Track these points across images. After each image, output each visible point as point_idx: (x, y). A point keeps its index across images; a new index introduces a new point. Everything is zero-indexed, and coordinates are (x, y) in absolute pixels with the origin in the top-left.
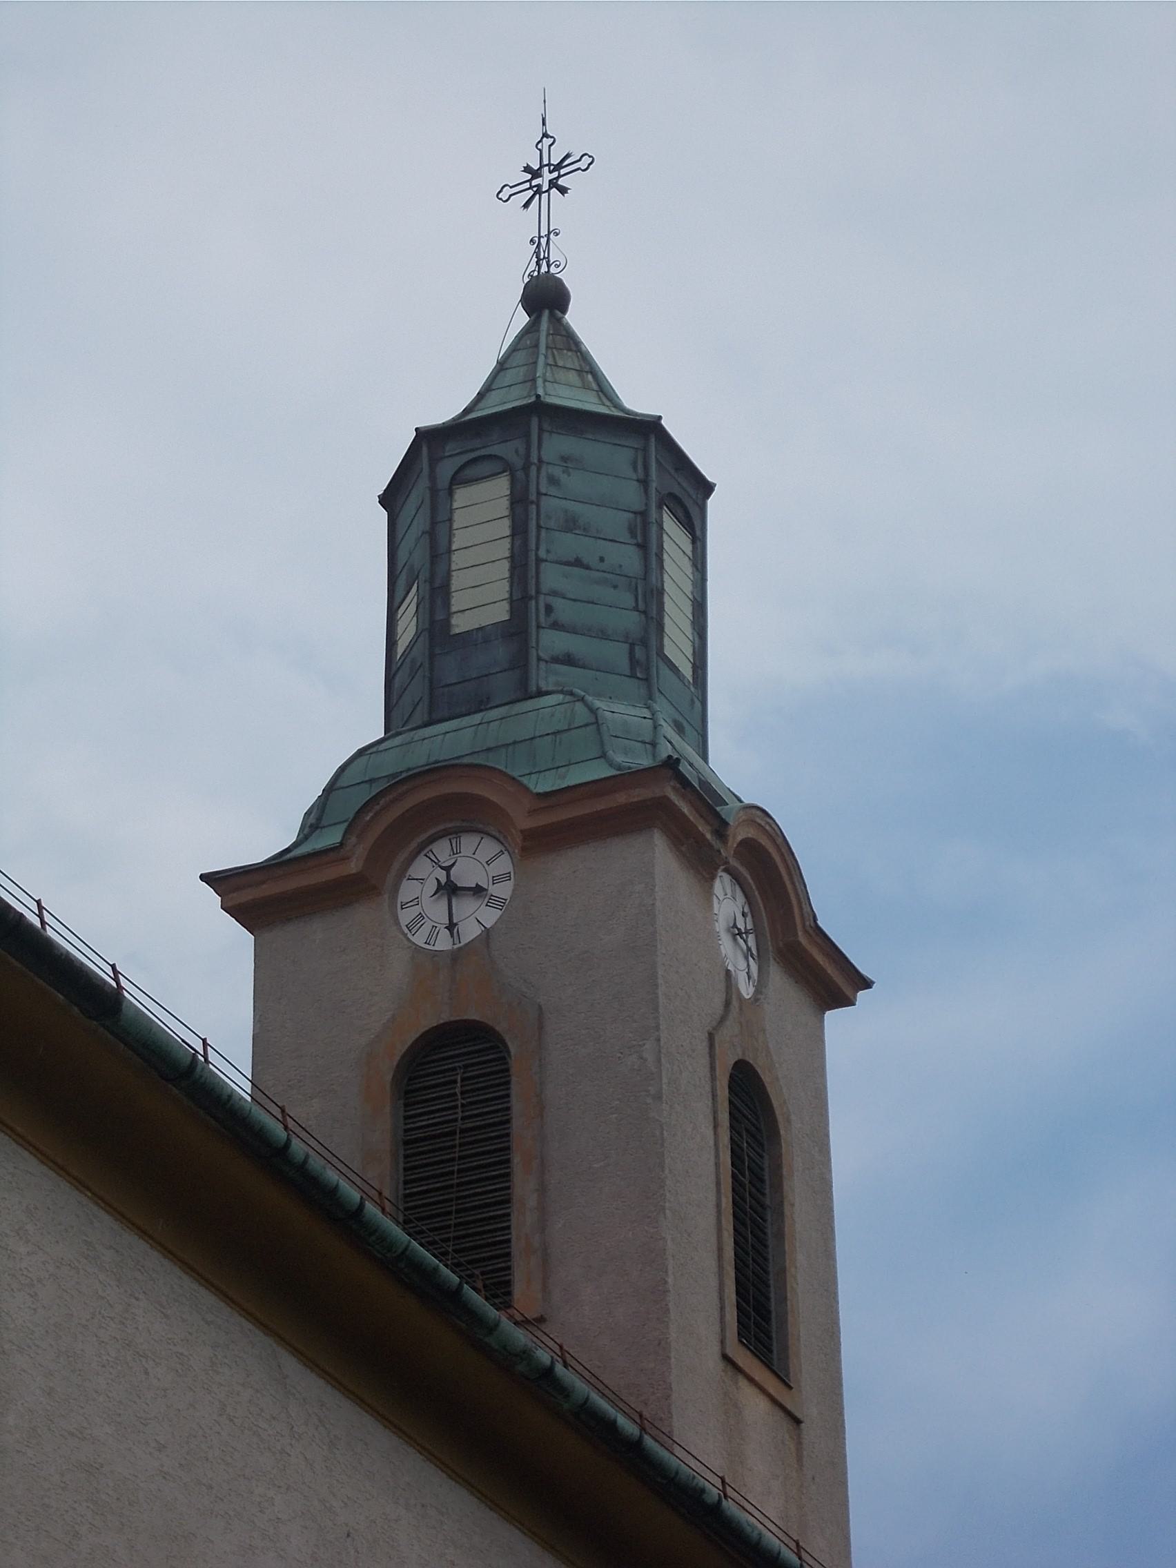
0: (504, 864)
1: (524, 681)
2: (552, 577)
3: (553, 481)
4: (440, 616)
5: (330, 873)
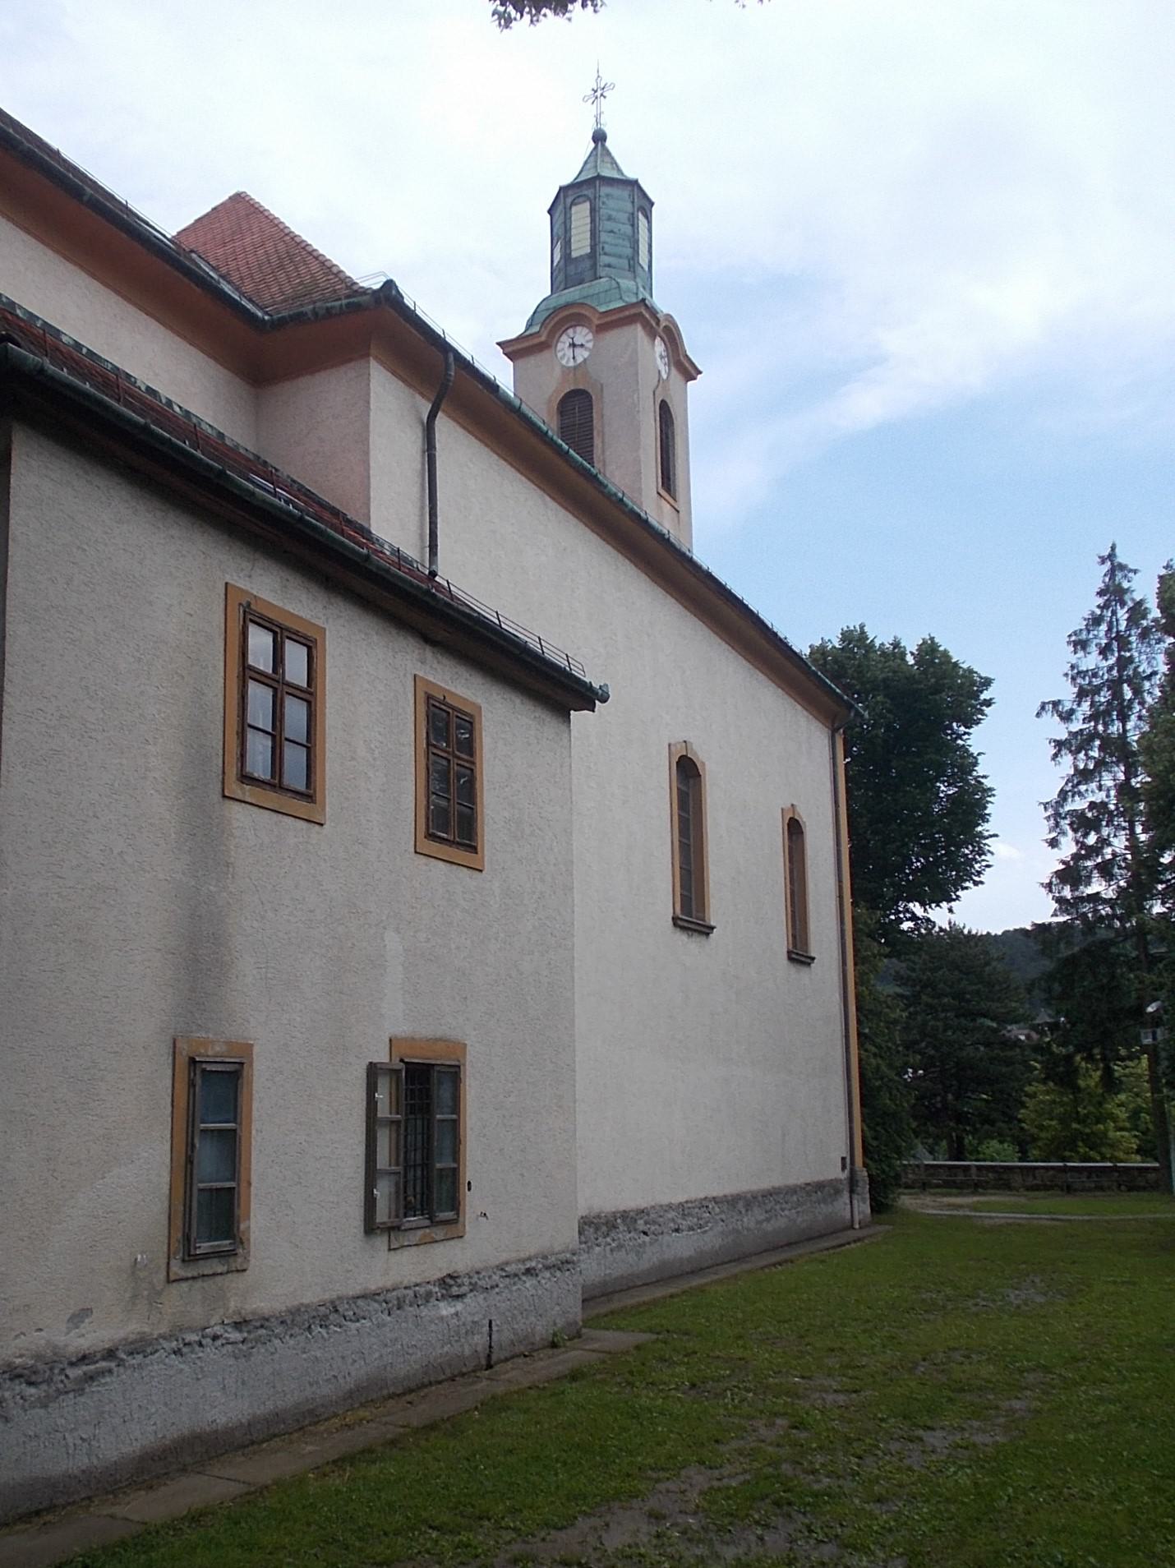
0: (590, 336)
1: (595, 273)
2: (604, 237)
3: (604, 203)
4: (568, 252)
5: (536, 341)
